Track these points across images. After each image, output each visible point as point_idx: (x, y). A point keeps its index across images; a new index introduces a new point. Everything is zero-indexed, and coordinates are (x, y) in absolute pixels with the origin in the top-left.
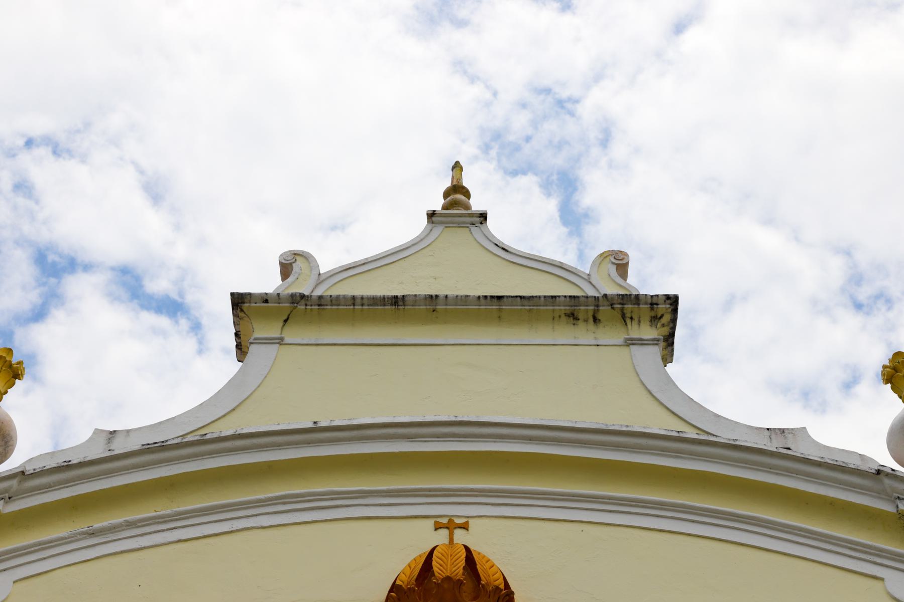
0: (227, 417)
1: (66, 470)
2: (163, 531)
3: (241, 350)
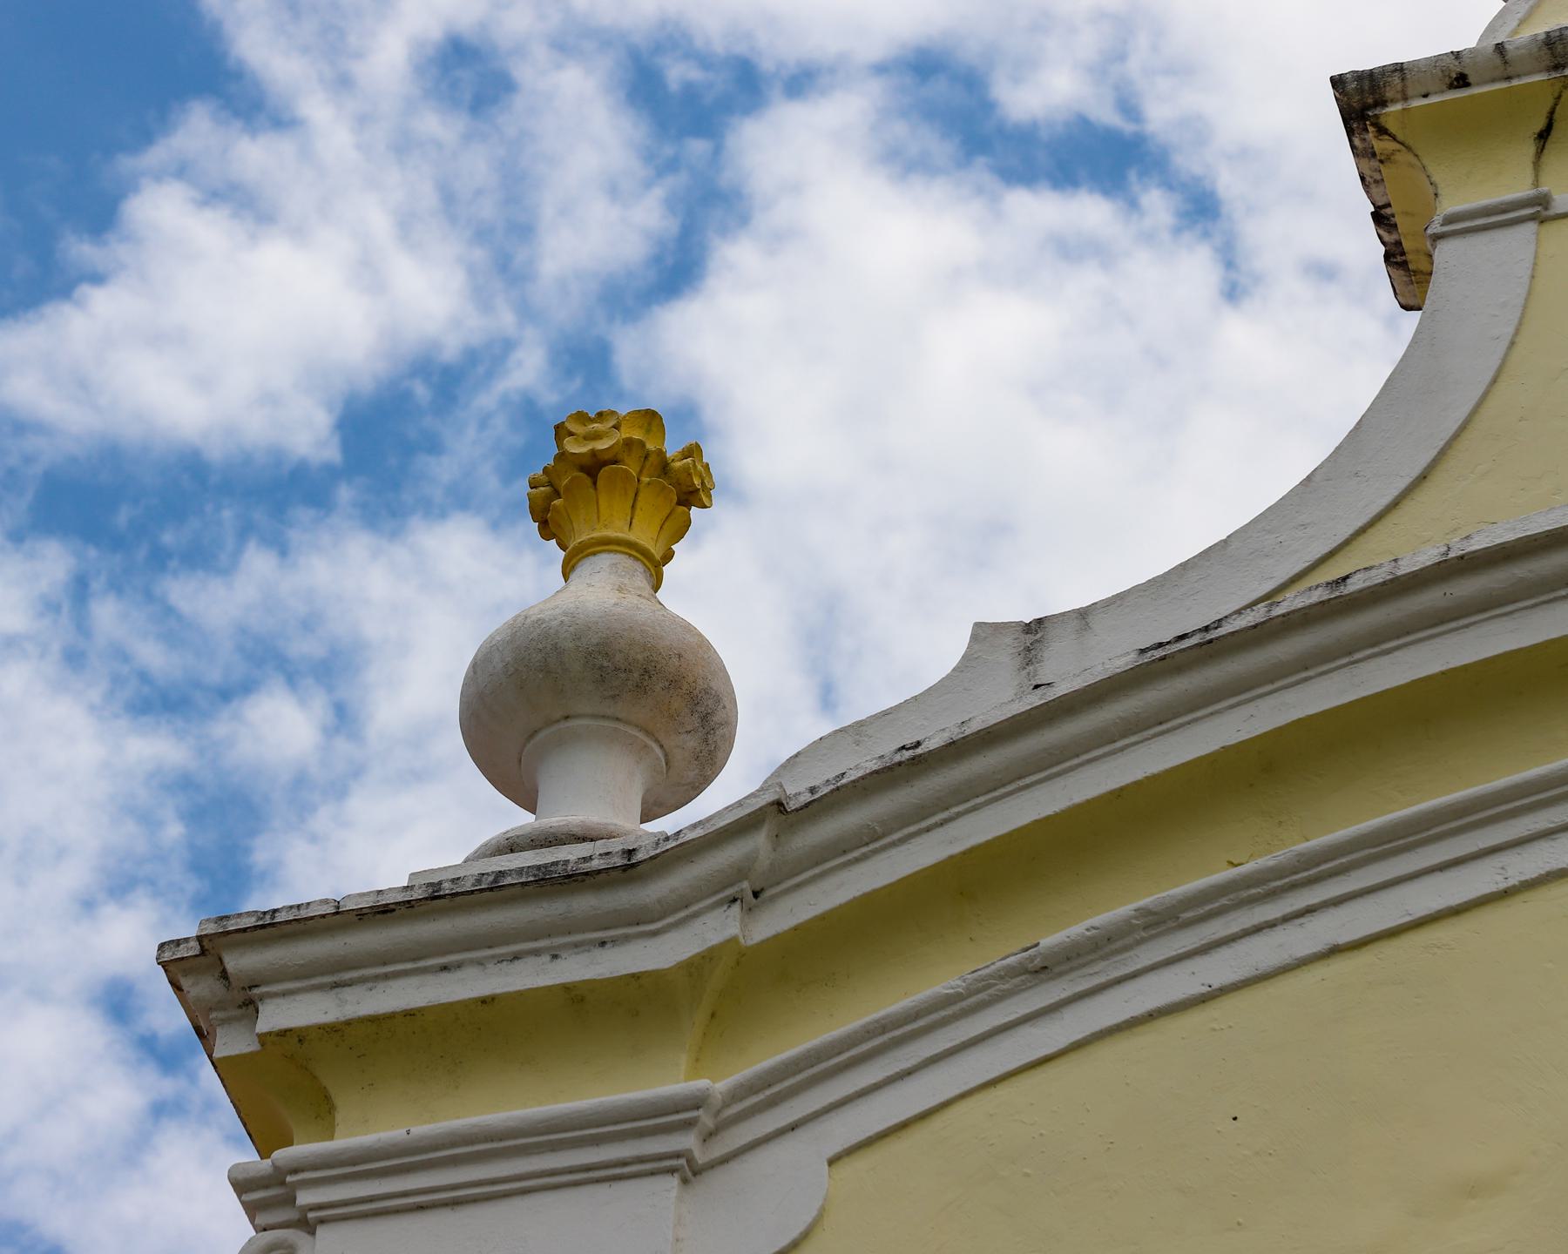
0: (1408, 507)
1: (909, 773)
2: (1272, 925)
3: (1408, 269)
